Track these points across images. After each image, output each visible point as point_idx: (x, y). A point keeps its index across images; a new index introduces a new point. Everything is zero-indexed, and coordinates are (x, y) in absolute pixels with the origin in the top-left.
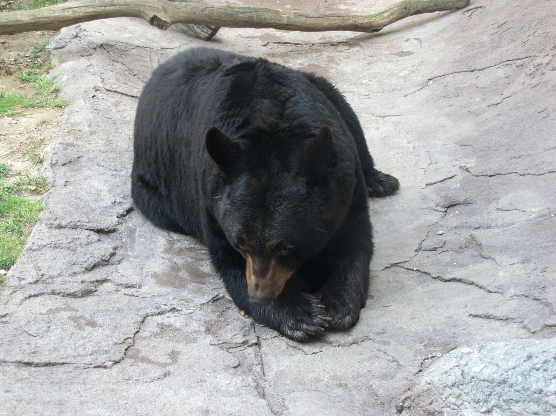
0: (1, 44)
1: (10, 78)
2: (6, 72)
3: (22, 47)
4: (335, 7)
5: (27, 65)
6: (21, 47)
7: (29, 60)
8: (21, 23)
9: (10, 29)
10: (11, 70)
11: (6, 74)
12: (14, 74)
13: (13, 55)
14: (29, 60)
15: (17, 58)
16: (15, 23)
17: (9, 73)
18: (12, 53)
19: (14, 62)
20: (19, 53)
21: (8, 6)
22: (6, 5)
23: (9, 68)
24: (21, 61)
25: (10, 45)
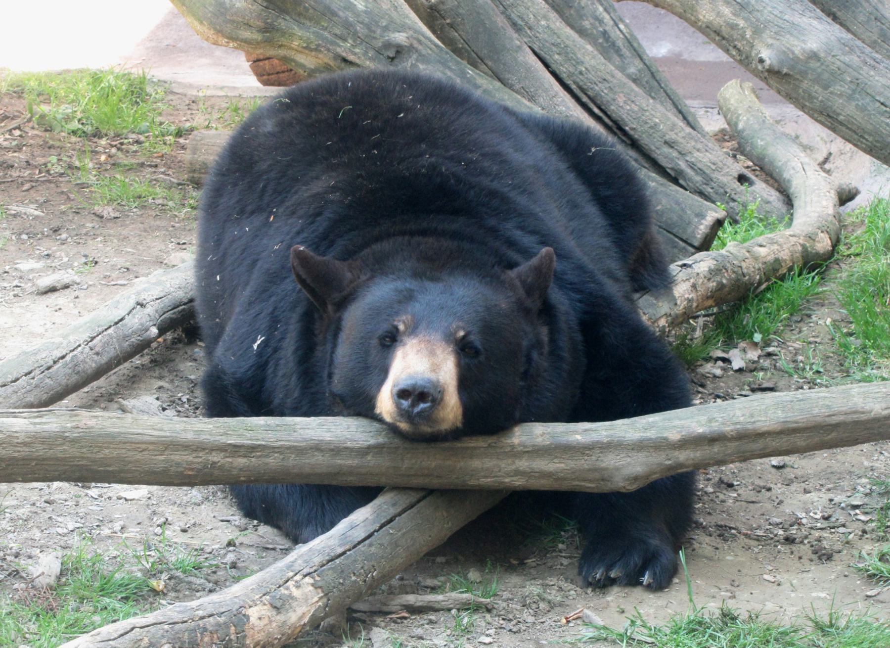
0: (774, 470)
1: (835, 568)
2: (815, 552)
3: (834, 478)
4: (492, 222)
5: (864, 532)
6: (831, 480)
7: (863, 518)
8: (864, 417)
9: (834, 435)
10: (825, 544)
11: (814, 557)
12: (836, 556)
13: (818, 500)
14: (863, 518)
15: (829, 512)
16: (849, 418)
17: (824, 556)
18: (813, 496)
19: (825, 524)
20: (831, 496)
21: (766, 363)
22: (759, 357)
23: (819, 540)
24: (842, 520)
25: (799, 473)
